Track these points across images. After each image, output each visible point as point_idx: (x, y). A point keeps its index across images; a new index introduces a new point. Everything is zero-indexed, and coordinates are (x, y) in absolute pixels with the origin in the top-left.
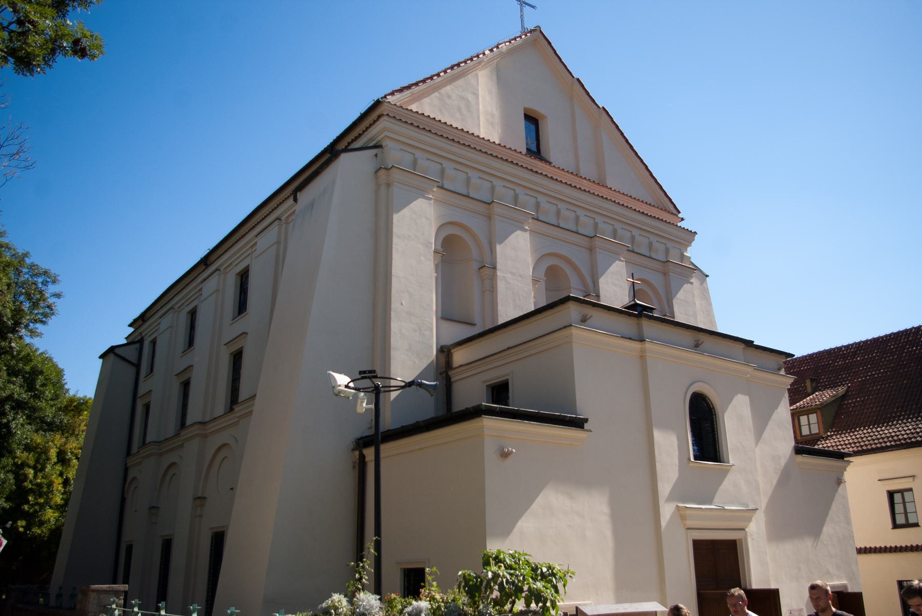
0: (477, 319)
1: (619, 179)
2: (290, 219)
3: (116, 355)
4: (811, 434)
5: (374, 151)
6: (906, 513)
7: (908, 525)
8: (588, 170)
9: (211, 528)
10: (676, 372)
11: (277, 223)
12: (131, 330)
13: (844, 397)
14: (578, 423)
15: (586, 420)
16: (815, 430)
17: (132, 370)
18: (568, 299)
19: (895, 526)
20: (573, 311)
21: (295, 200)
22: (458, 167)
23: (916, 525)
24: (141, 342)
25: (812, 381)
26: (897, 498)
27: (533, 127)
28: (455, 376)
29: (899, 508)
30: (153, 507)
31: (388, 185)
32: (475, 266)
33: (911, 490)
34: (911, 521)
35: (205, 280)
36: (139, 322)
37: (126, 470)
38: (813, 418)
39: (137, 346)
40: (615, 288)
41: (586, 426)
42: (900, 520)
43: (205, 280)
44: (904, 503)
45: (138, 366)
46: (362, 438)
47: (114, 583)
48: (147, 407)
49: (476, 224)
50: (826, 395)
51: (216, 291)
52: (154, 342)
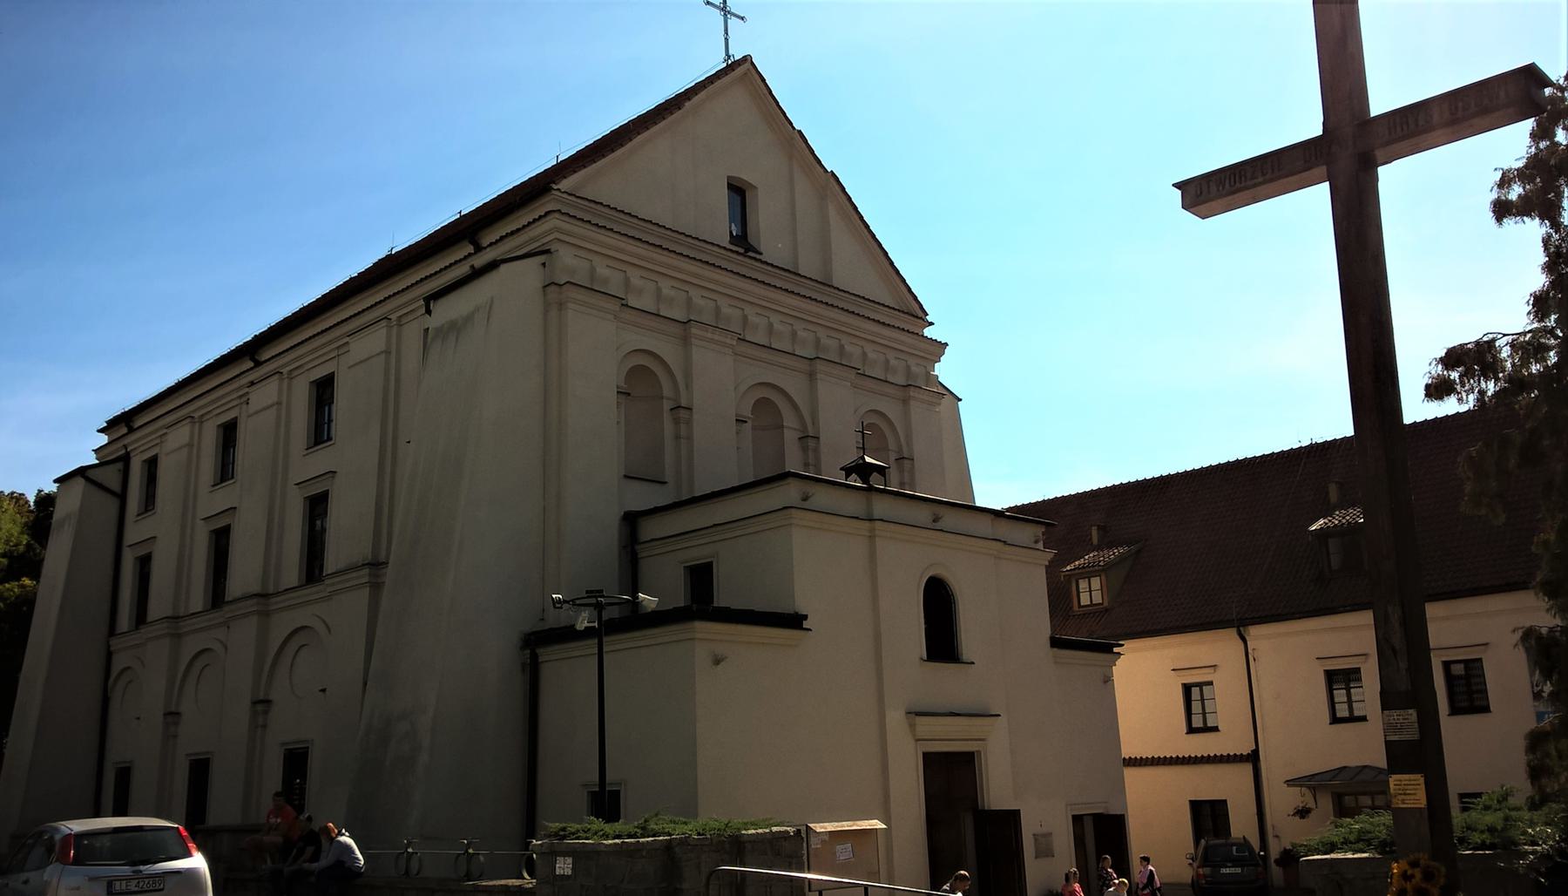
0: (669, 475)
1: (849, 272)
2: (404, 320)
3: (88, 479)
4: (1092, 605)
5: (542, 258)
6: (1204, 714)
7: (1206, 729)
8: (809, 265)
9: (283, 744)
10: (905, 566)
11: (384, 323)
12: (103, 439)
13: (1139, 551)
14: (794, 621)
15: (805, 617)
16: (1097, 598)
17: (112, 505)
18: (785, 476)
19: (1191, 730)
20: (789, 492)
21: (429, 312)
22: (645, 274)
23: (1215, 729)
24: (125, 459)
25: (1099, 528)
26: (1195, 692)
27: (738, 199)
28: (643, 552)
29: (1196, 707)
30: (171, 713)
31: (561, 305)
32: (667, 405)
33: (1211, 683)
34: (1356, 713)
35: (252, 383)
36: (120, 424)
37: (109, 655)
38: (1096, 583)
39: (120, 465)
40: (838, 447)
41: (806, 624)
42: (1197, 722)
43: (252, 383)
44: (1203, 700)
45: (122, 497)
46: (534, 633)
47: (97, 814)
48: (145, 562)
49: (667, 349)
50: (1114, 553)
51: (279, 403)
52: (152, 464)
